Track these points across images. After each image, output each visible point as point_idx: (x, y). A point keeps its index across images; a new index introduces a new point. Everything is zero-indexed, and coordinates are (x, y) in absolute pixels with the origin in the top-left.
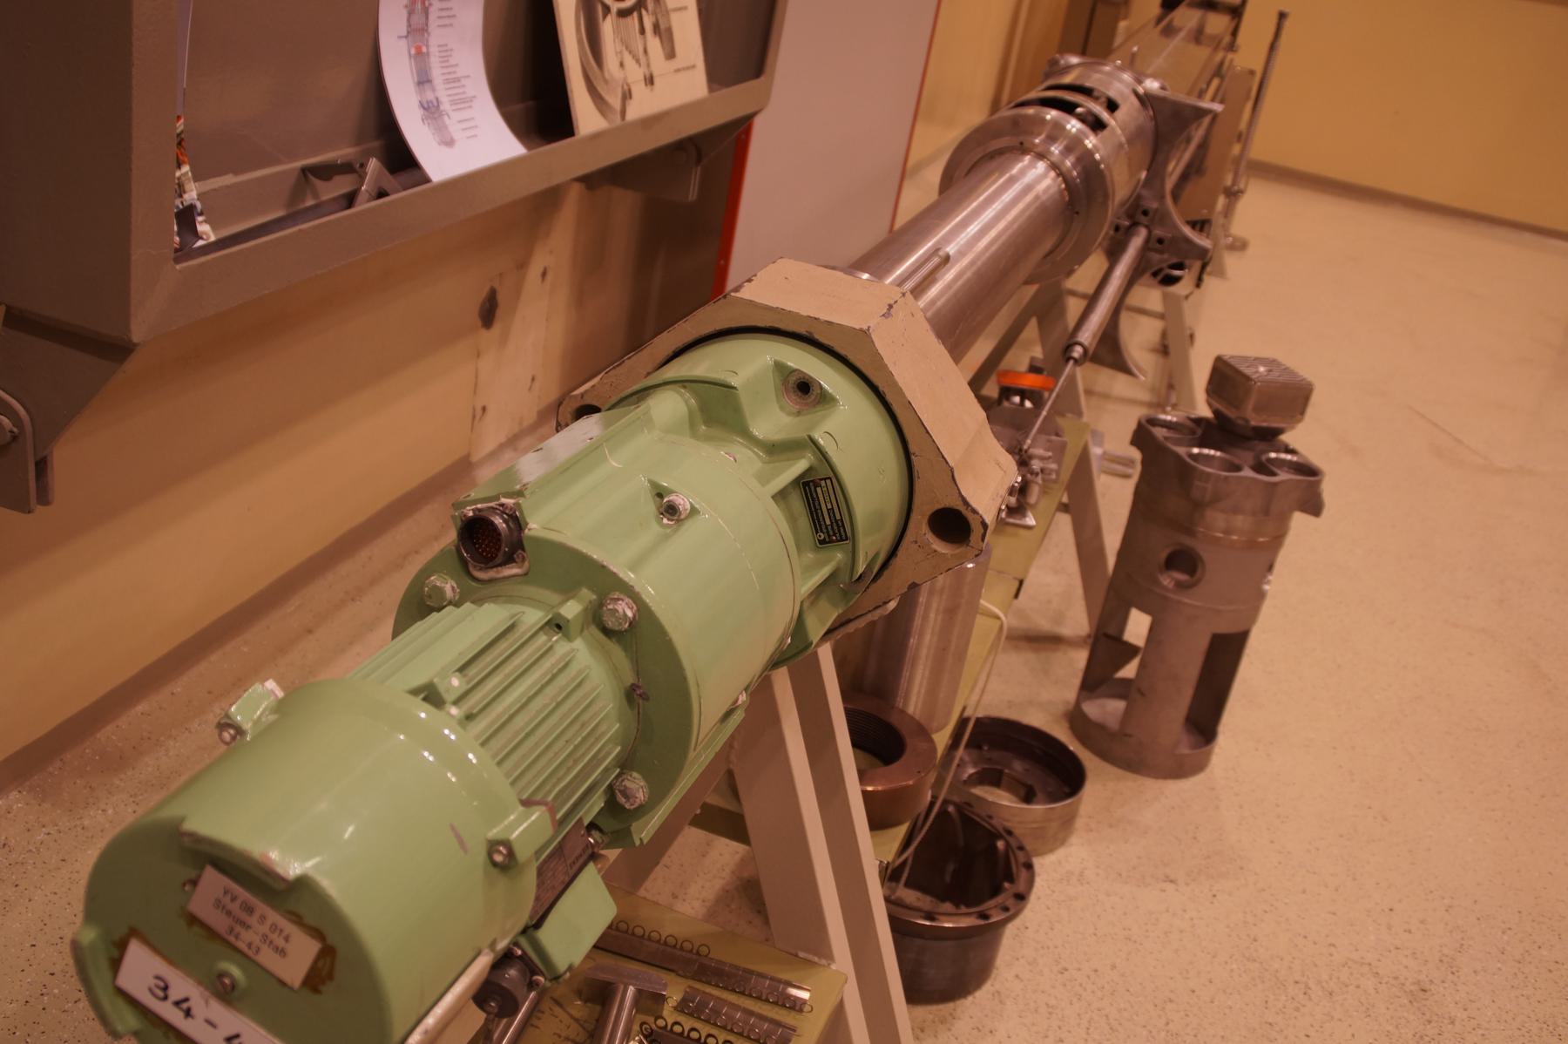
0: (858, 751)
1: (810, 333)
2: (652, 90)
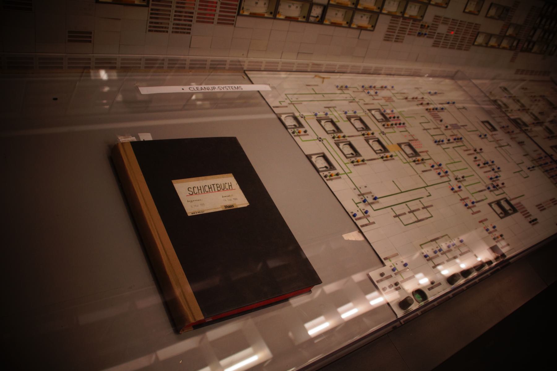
0: (412, 293)
1: (237, 184)
2: (335, 85)
